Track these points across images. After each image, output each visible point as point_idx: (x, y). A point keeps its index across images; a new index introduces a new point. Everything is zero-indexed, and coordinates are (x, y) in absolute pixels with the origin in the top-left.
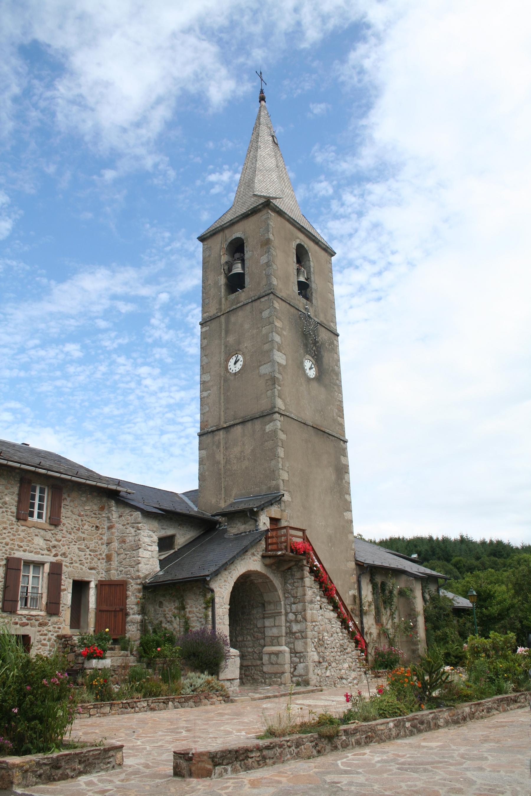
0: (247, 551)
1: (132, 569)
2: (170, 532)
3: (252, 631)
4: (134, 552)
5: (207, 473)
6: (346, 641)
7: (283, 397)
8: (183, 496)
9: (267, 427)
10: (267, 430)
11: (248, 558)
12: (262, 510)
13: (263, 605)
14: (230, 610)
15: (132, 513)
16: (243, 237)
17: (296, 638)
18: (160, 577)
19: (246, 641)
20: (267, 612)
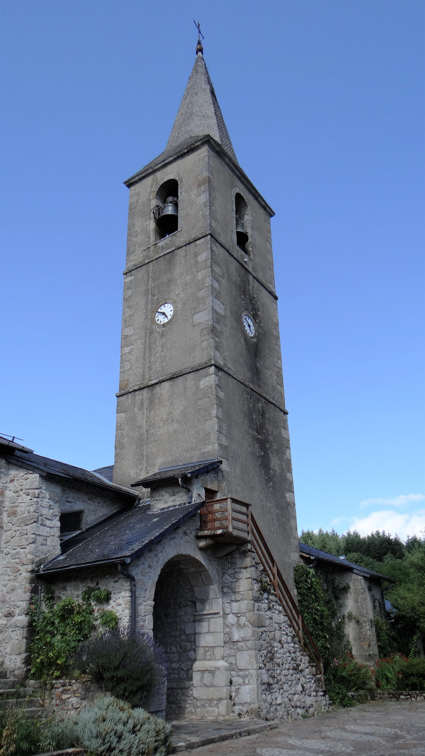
0: (178, 528)
1: (22, 550)
2: (77, 506)
3: (178, 639)
4: (26, 527)
5: (126, 439)
6: (298, 654)
7: (221, 350)
8: (94, 473)
9: (202, 383)
10: (202, 386)
11: (179, 538)
12: (197, 477)
13: (194, 603)
14: (155, 607)
15: (28, 476)
16: (177, 179)
17: (239, 650)
18: (59, 562)
19: (170, 653)
20: (198, 613)
